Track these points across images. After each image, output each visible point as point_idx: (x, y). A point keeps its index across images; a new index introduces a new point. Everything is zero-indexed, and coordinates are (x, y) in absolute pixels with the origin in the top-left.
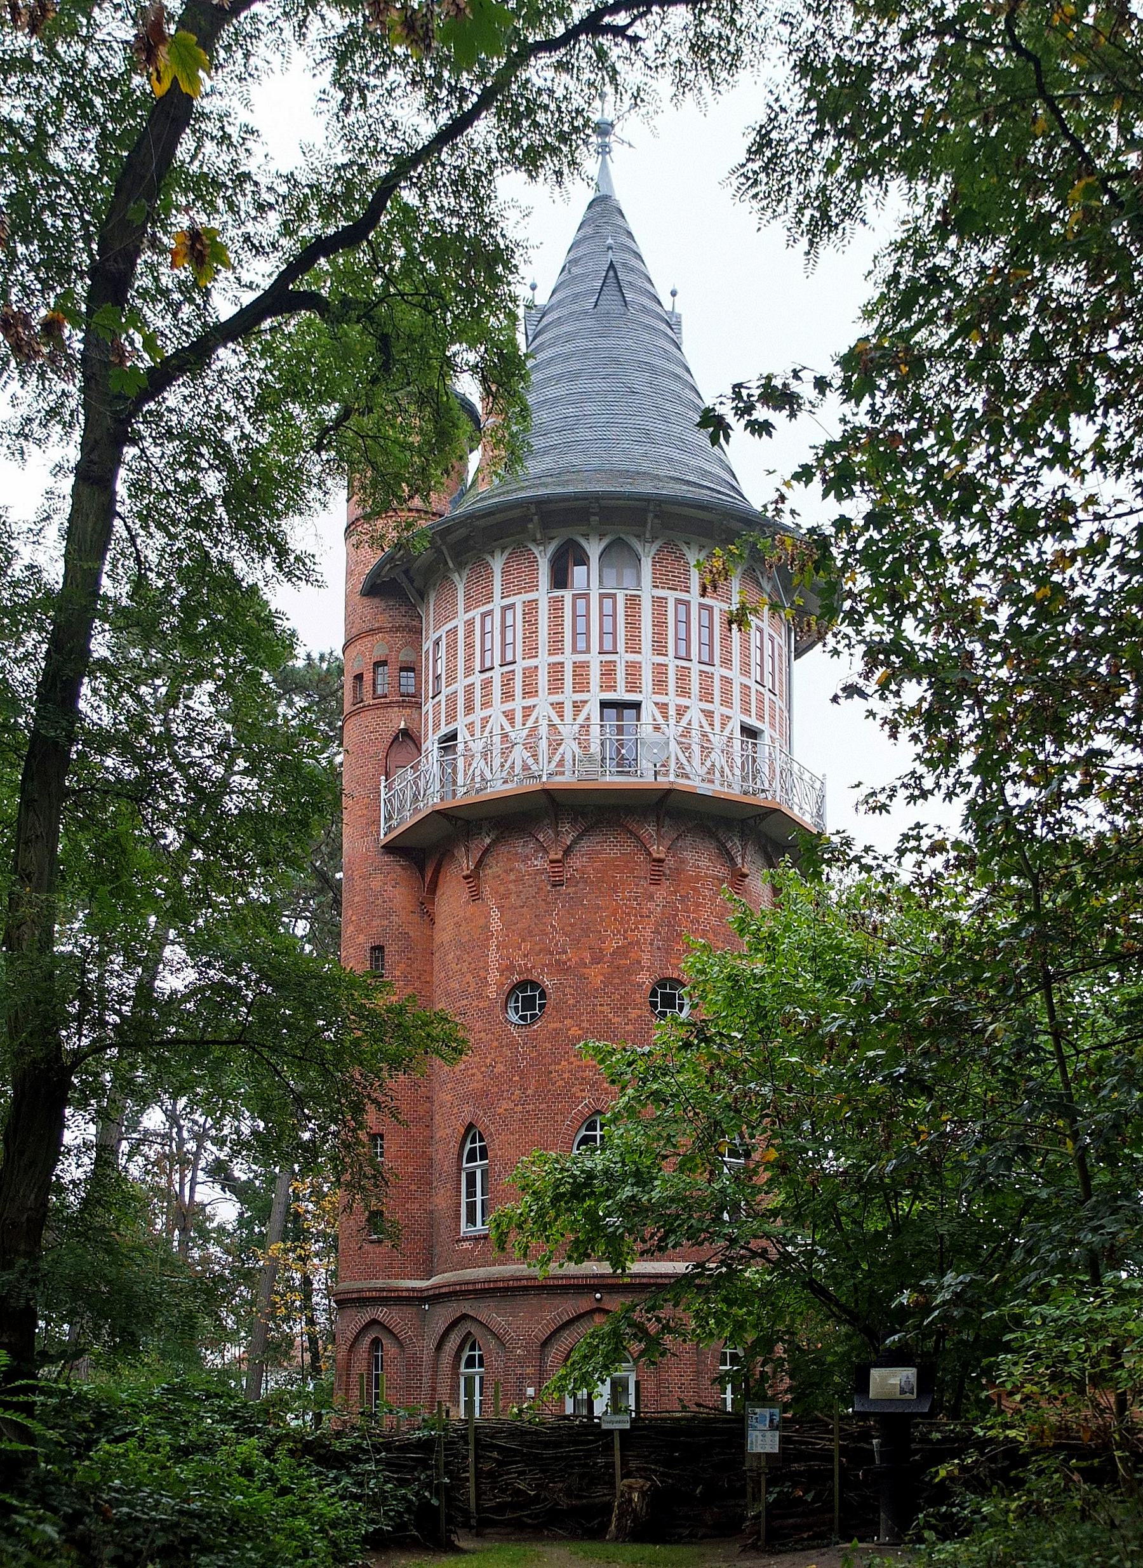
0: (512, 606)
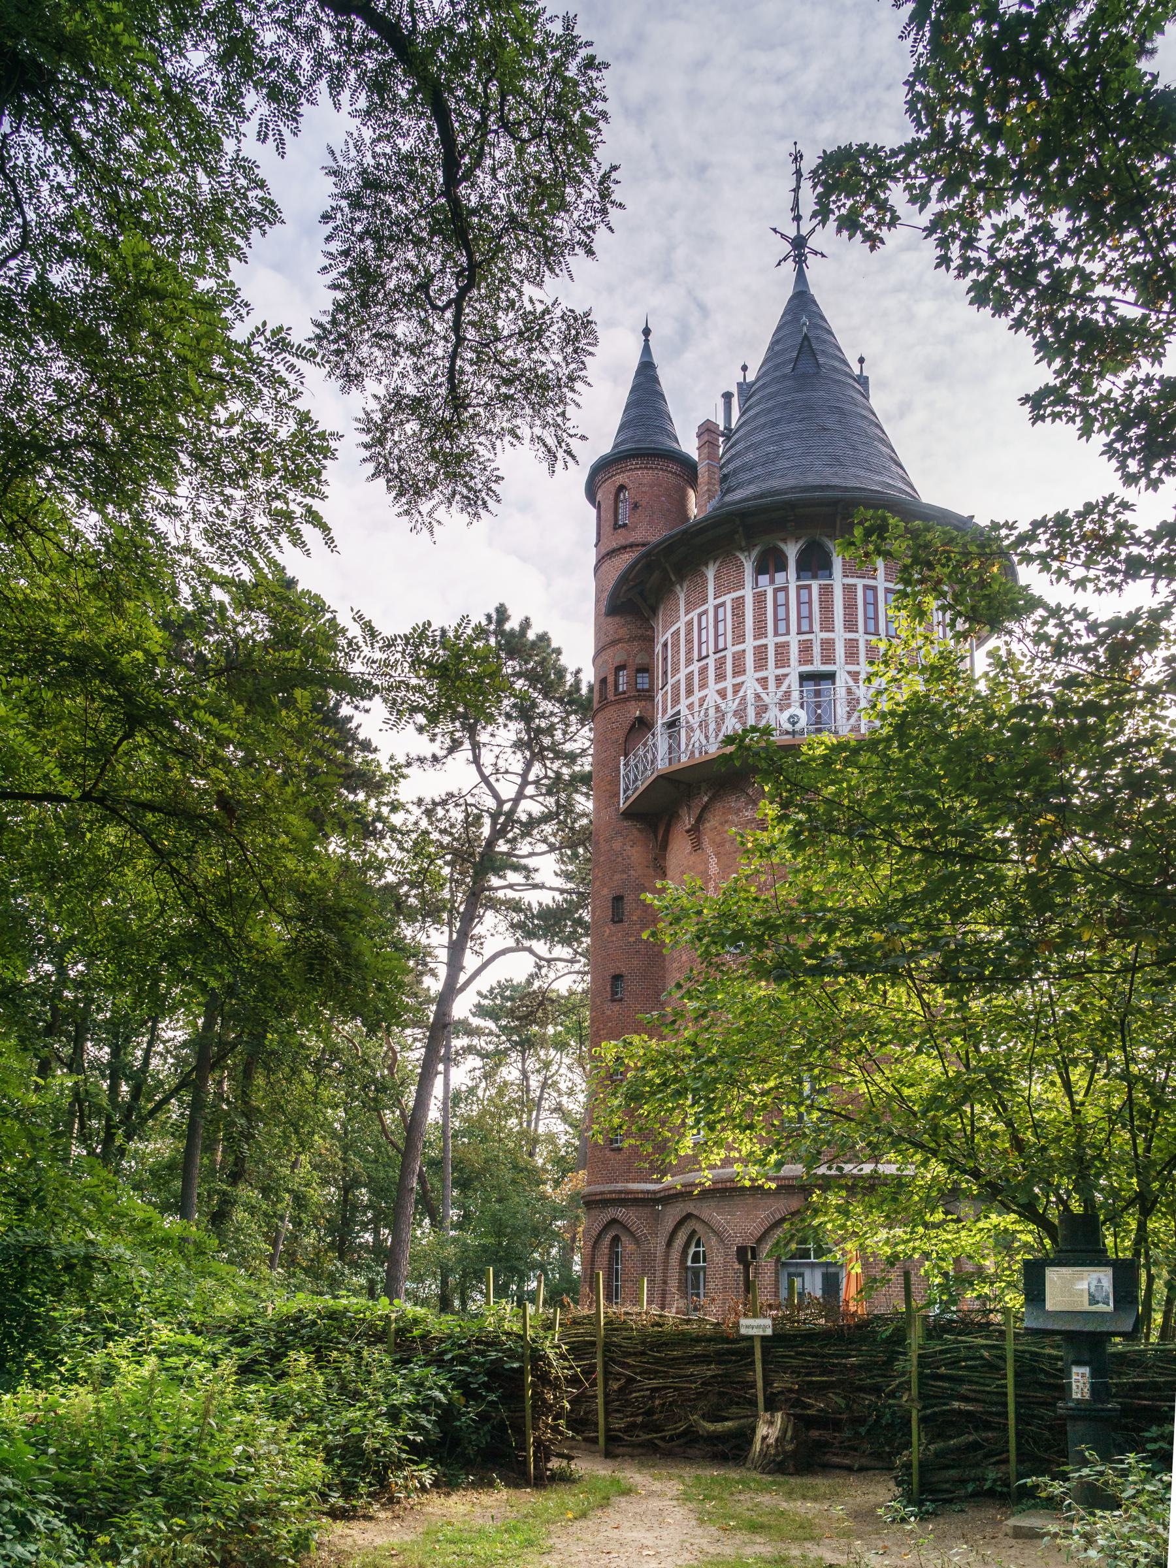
0: (723, 604)
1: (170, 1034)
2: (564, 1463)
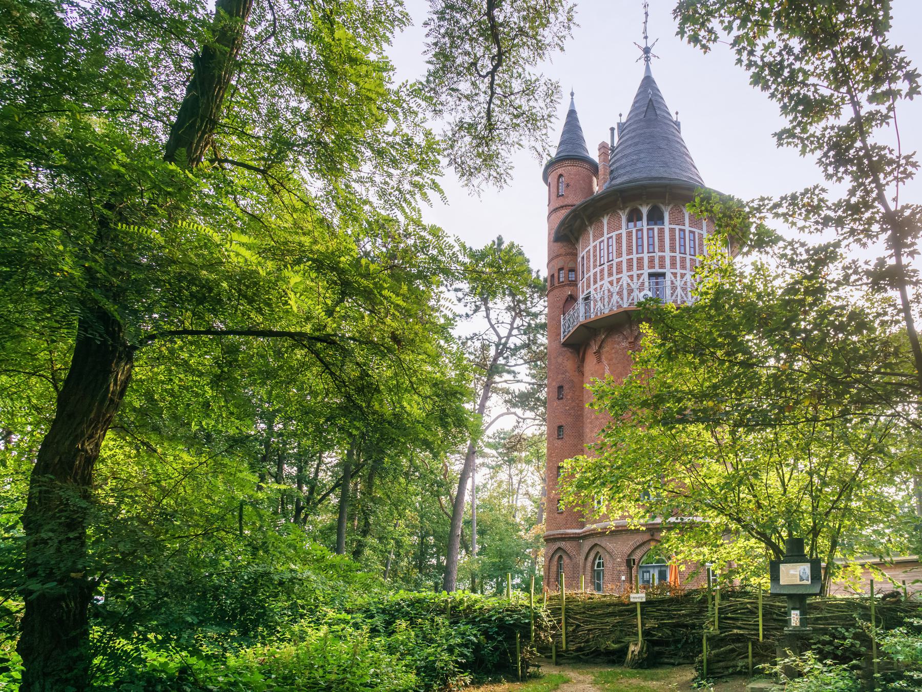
0: (611, 237)
1: (329, 460)
2: (536, 669)
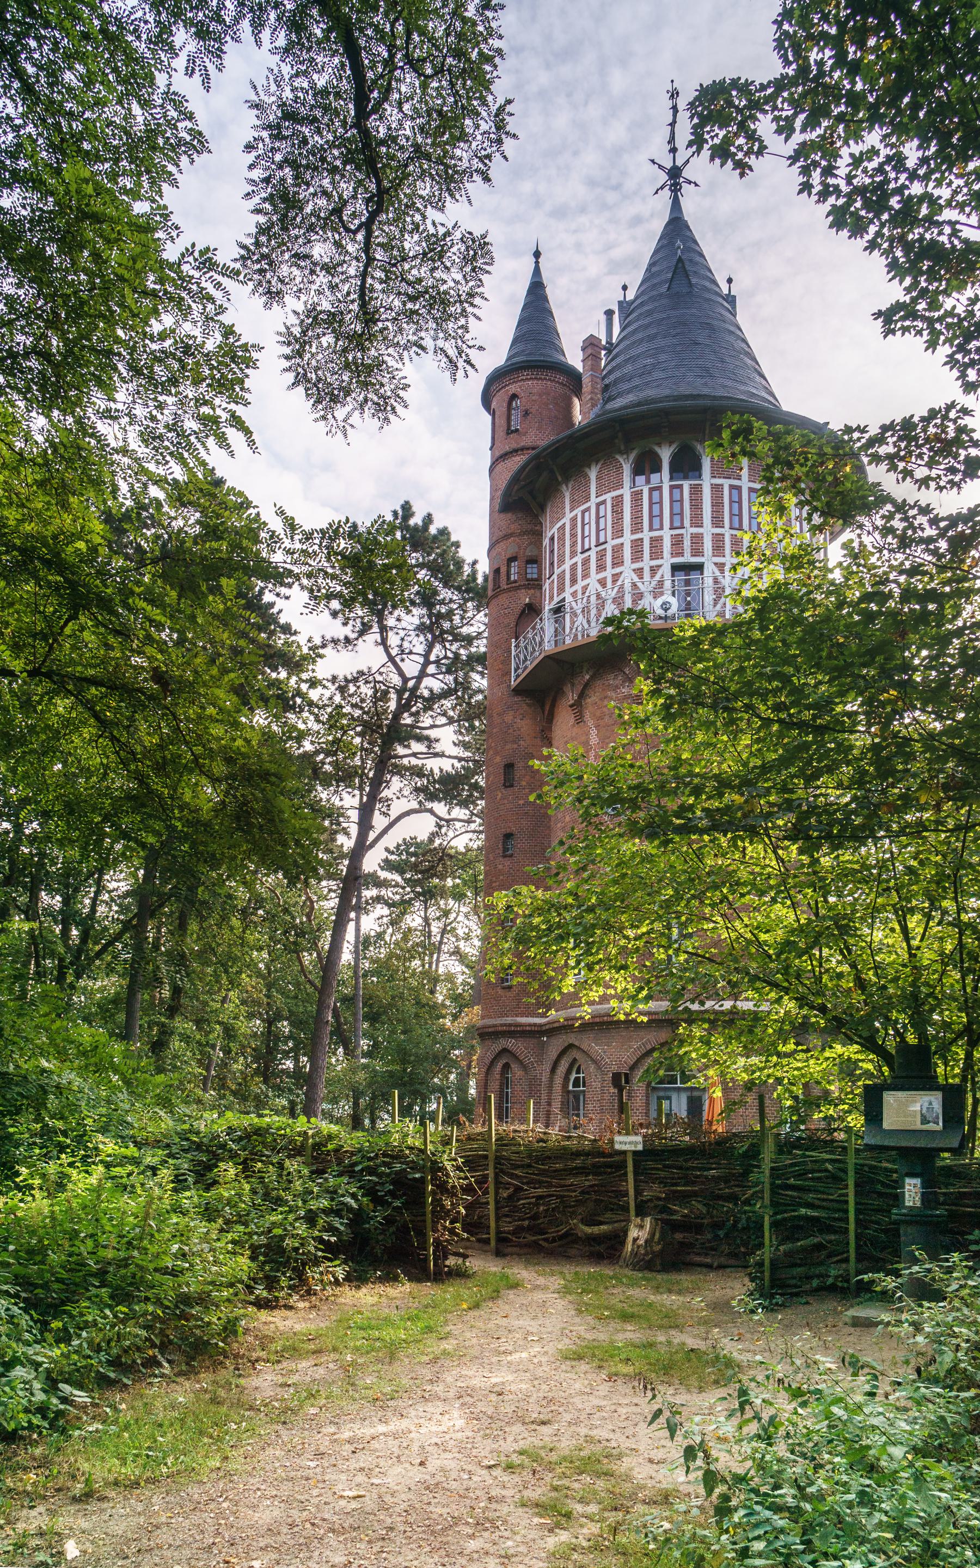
0: (604, 502)
2: (460, 1261)
